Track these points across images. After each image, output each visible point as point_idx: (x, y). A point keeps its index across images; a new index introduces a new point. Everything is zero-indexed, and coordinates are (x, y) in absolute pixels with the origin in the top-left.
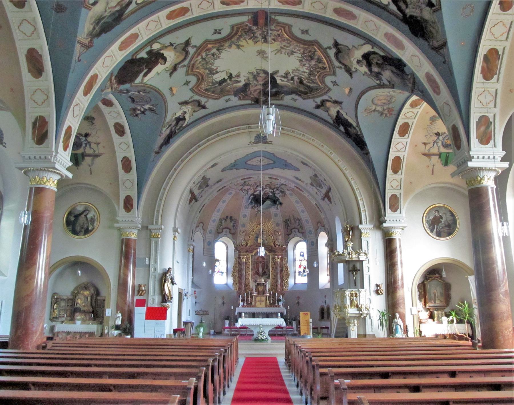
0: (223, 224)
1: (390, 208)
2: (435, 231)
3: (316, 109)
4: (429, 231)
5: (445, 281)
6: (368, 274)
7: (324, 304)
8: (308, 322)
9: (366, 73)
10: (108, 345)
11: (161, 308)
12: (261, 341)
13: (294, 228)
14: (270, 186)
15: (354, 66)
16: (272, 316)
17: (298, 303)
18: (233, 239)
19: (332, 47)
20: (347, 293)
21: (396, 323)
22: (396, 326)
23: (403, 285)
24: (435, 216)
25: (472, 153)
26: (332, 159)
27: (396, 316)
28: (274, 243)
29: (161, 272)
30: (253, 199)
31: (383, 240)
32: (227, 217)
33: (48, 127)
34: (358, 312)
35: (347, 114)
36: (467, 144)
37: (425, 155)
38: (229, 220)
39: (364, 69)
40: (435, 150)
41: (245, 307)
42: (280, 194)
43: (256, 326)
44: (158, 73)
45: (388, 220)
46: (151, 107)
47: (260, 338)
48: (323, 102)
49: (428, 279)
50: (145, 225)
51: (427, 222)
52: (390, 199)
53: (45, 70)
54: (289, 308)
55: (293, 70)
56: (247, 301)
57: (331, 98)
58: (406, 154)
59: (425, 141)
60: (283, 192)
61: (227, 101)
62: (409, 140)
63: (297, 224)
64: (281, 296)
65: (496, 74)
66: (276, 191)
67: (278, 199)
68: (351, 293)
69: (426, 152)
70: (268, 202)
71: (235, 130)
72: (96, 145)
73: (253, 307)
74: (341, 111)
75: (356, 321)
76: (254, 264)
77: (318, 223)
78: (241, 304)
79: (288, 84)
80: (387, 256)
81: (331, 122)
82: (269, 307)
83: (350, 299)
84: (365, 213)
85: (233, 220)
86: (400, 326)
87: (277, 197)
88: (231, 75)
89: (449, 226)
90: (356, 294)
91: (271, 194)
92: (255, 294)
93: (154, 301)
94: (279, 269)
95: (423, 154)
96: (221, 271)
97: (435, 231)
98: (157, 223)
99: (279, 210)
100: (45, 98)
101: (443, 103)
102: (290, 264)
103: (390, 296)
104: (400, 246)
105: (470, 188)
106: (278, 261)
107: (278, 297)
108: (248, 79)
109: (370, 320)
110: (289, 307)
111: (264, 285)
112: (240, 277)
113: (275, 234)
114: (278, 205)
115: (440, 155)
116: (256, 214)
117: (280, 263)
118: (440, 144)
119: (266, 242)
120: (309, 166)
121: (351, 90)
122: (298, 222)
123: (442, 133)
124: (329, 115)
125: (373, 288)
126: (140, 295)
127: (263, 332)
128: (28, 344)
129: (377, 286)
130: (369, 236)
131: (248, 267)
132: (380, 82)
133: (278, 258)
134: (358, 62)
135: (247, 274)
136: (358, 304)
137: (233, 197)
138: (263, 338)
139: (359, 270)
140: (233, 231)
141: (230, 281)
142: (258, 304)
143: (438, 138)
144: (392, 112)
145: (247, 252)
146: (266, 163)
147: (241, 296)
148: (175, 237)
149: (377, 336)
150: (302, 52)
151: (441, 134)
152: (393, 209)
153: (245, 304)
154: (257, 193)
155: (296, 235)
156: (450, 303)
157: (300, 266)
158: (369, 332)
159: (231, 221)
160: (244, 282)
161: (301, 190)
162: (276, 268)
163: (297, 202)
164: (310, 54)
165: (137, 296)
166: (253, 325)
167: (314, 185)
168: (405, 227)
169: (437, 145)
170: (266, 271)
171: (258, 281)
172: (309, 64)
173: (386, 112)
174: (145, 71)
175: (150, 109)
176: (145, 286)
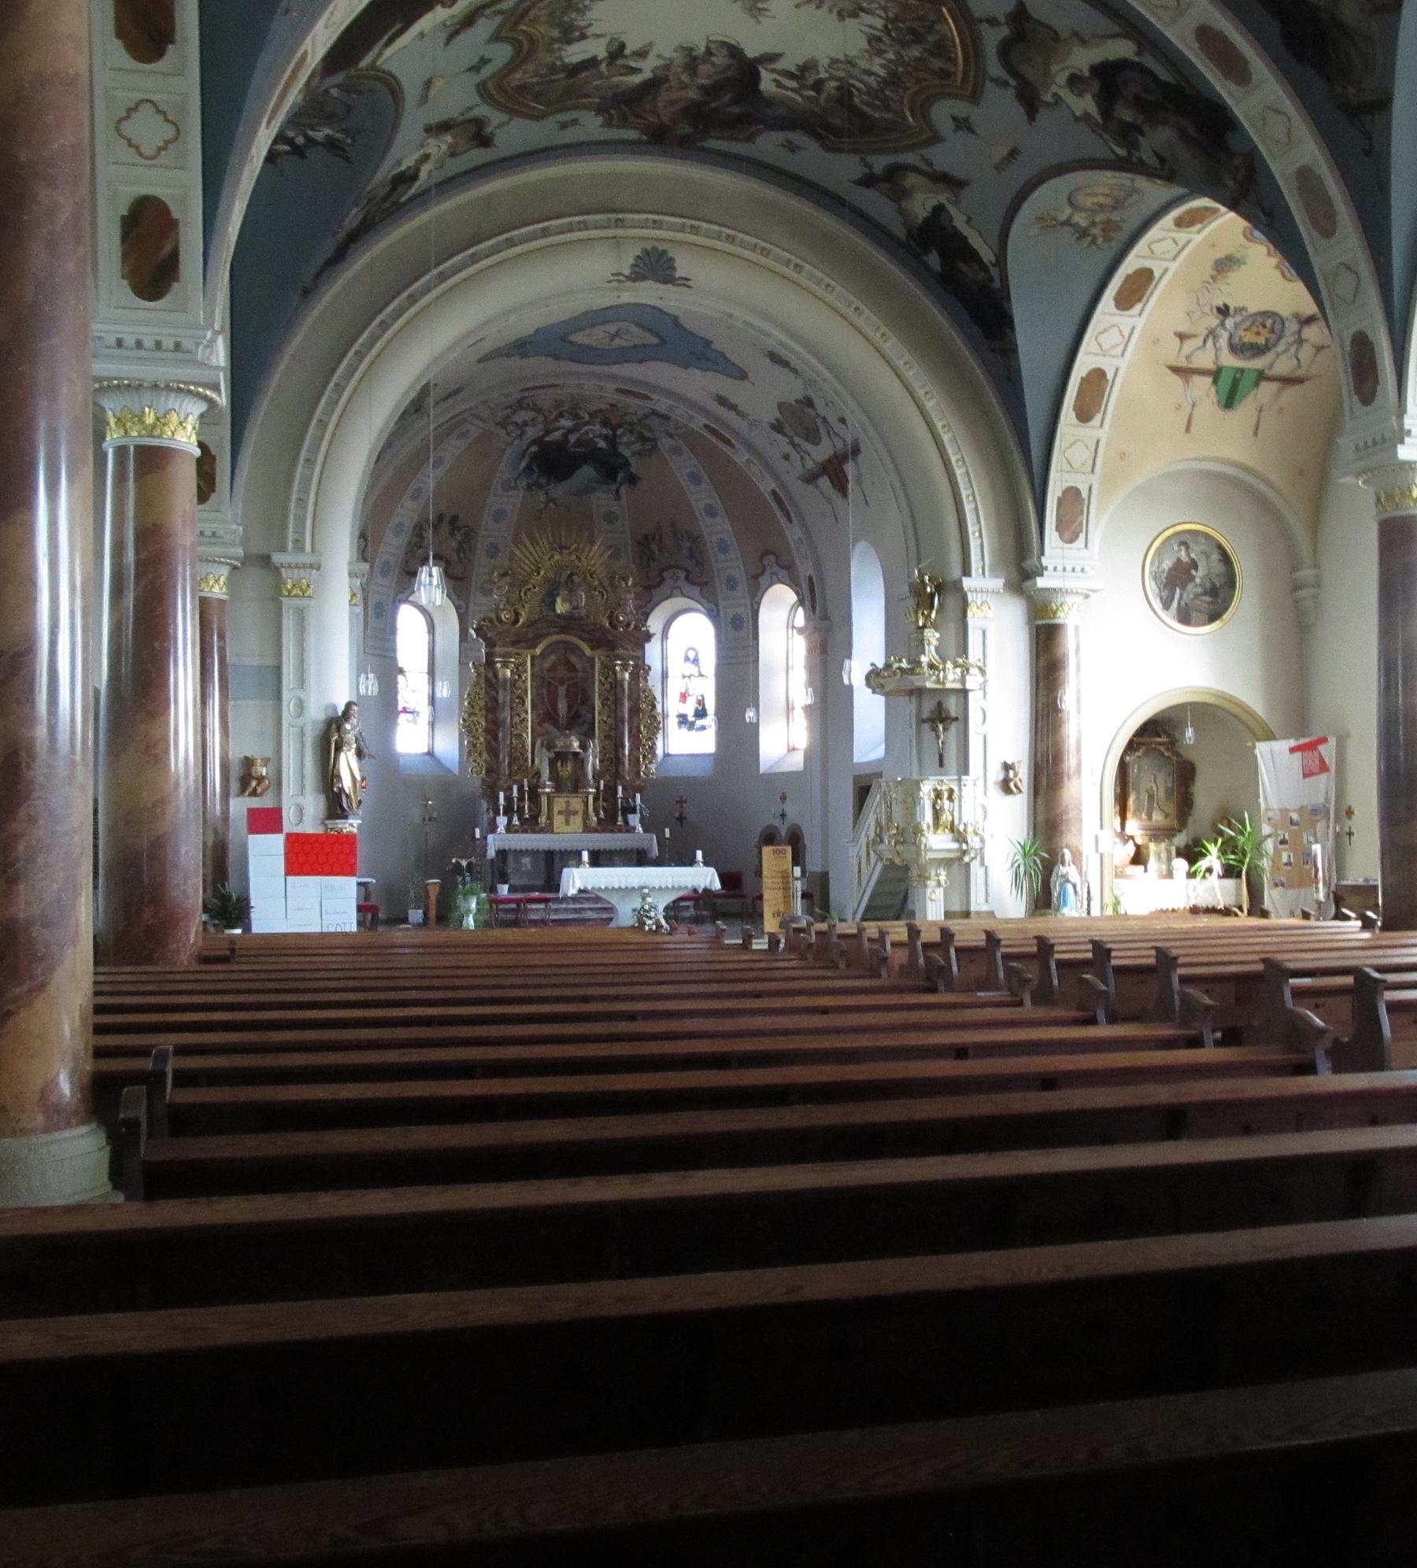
3: (862, 189)
4: (1157, 605)
5: (1181, 756)
6: (983, 730)
7: (777, 822)
9: (1086, 117)
10: (322, 948)
11: (327, 836)
14: (609, 419)
15: (1054, 89)
16: (610, 859)
19: (1002, 20)
20: (926, 789)
21: (1063, 876)
22: (1062, 885)
23: (1079, 765)
25: (1045, 561)
26: (883, 357)
27: (1063, 856)
30: (535, 457)
31: (1026, 629)
33: (177, 239)
34: (955, 846)
35: (969, 221)
36: (1397, 396)
37: (1176, 370)
38: (445, 528)
39: (1086, 104)
40: (1205, 360)
41: (516, 832)
42: (637, 447)
43: (627, 891)
44: (422, 35)
45: (1050, 567)
46: (338, 135)
48: (894, 174)
49: (1138, 749)
50: (256, 548)
51: (1155, 577)
52: (1060, 502)
53: (178, 37)
54: (667, 835)
55: (834, 62)
56: (521, 810)
57: (931, 165)
58: (1123, 364)
59: (1183, 328)
60: (648, 439)
61: (564, 126)
62: (1140, 323)
64: (638, 796)
66: (623, 434)
67: (627, 464)
68: (935, 790)
69: (1182, 362)
70: (587, 472)
71: (570, 229)
73: (542, 831)
74: (950, 208)
75: (943, 873)
76: (537, 688)
78: (502, 821)
79: (797, 98)
80: (1037, 679)
81: (901, 233)
82: (596, 831)
85: (459, 531)
86: (1074, 886)
87: (624, 457)
88: (622, 46)
89: (1213, 592)
90: (951, 791)
91: (602, 444)
92: (547, 790)
93: (300, 812)
98: (299, 546)
99: (624, 502)
100: (170, 132)
101: (1334, 264)
103: (1040, 800)
104: (1077, 650)
105: (1385, 516)
106: (623, 680)
107: (625, 798)
108: (667, 67)
109: (983, 869)
111: (578, 760)
112: (492, 732)
114: (621, 484)
115: (1216, 374)
116: (540, 511)
117: (629, 683)
118: (1223, 342)
119: (583, 613)
120: (795, 371)
121: (1014, 153)
124: (901, 212)
125: (996, 774)
126: (249, 795)
128: (178, 951)
129: (1007, 767)
130: (990, 614)
131: (519, 697)
132: (1130, 154)
133: (625, 667)
134: (1074, 81)
135: (517, 719)
136: (956, 822)
139: (956, 719)
142: (558, 820)
144: (1112, 234)
145: (514, 644)
146: (632, 344)
149: (999, 915)
150: (891, 15)
151: (1231, 312)
152: (1067, 535)
153: (516, 821)
154: (557, 435)
155: (676, 591)
156: (1191, 820)
157: (684, 697)
158: (977, 903)
159: (452, 534)
160: (507, 750)
161: (729, 443)
162: (618, 702)
163: (695, 479)
164: (915, 25)
165: (238, 795)
166: (620, 888)
167: (787, 429)
168: (1094, 591)
170: (583, 711)
171: (559, 743)
172: (898, 53)
173: (1096, 231)
174: (398, 26)
175: (331, 144)
176: (266, 762)
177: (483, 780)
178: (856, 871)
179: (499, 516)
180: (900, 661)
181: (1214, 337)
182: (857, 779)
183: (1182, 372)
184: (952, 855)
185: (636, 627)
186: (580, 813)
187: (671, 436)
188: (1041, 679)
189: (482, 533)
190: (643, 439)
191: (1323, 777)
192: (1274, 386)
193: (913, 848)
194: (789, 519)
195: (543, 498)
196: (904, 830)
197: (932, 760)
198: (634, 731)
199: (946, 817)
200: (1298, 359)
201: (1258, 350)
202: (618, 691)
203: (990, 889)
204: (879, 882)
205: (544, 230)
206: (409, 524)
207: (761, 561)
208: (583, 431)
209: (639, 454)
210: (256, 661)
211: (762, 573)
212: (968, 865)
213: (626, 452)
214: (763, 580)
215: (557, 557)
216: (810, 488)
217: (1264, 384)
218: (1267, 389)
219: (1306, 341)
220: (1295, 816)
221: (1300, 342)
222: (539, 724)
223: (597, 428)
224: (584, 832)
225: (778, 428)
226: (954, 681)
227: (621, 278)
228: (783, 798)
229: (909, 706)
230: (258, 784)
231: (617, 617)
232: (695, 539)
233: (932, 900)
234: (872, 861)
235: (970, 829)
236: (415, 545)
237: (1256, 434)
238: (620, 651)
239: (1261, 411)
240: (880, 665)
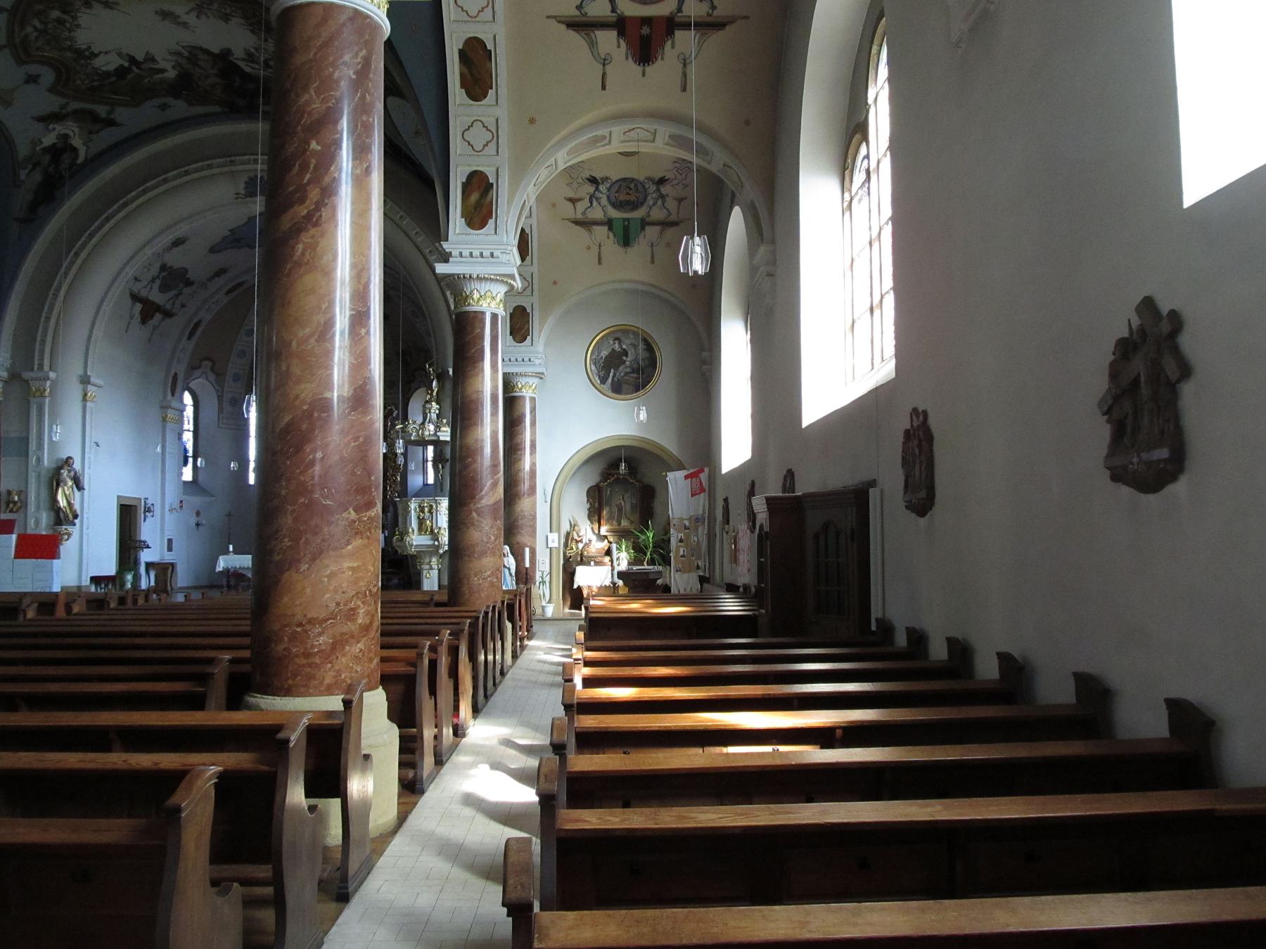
2: (610, 380)
24: (613, 349)
29: (54, 466)
37: (577, 223)
40: (597, 213)
51: (595, 362)
65: (492, 88)
68: (420, 506)
71: (201, 169)
72: (675, 203)
83: (419, 517)
93: (37, 523)
95: (573, 222)
97: (610, 380)
98: (41, 366)
115: (609, 223)
118: (604, 201)
123: (602, 179)
136: (434, 527)
143: (597, 189)
165: (5, 512)
169: (599, 204)
181: (597, 199)
183: (585, 224)
191: (702, 495)
192: (658, 228)
200: (666, 208)
201: (634, 206)
205: (186, 171)
207: (201, 361)
217: (648, 228)
218: (652, 232)
219: (667, 195)
220: (687, 523)
221: (663, 197)
227: (242, 196)
237: (653, 262)
239: (652, 246)
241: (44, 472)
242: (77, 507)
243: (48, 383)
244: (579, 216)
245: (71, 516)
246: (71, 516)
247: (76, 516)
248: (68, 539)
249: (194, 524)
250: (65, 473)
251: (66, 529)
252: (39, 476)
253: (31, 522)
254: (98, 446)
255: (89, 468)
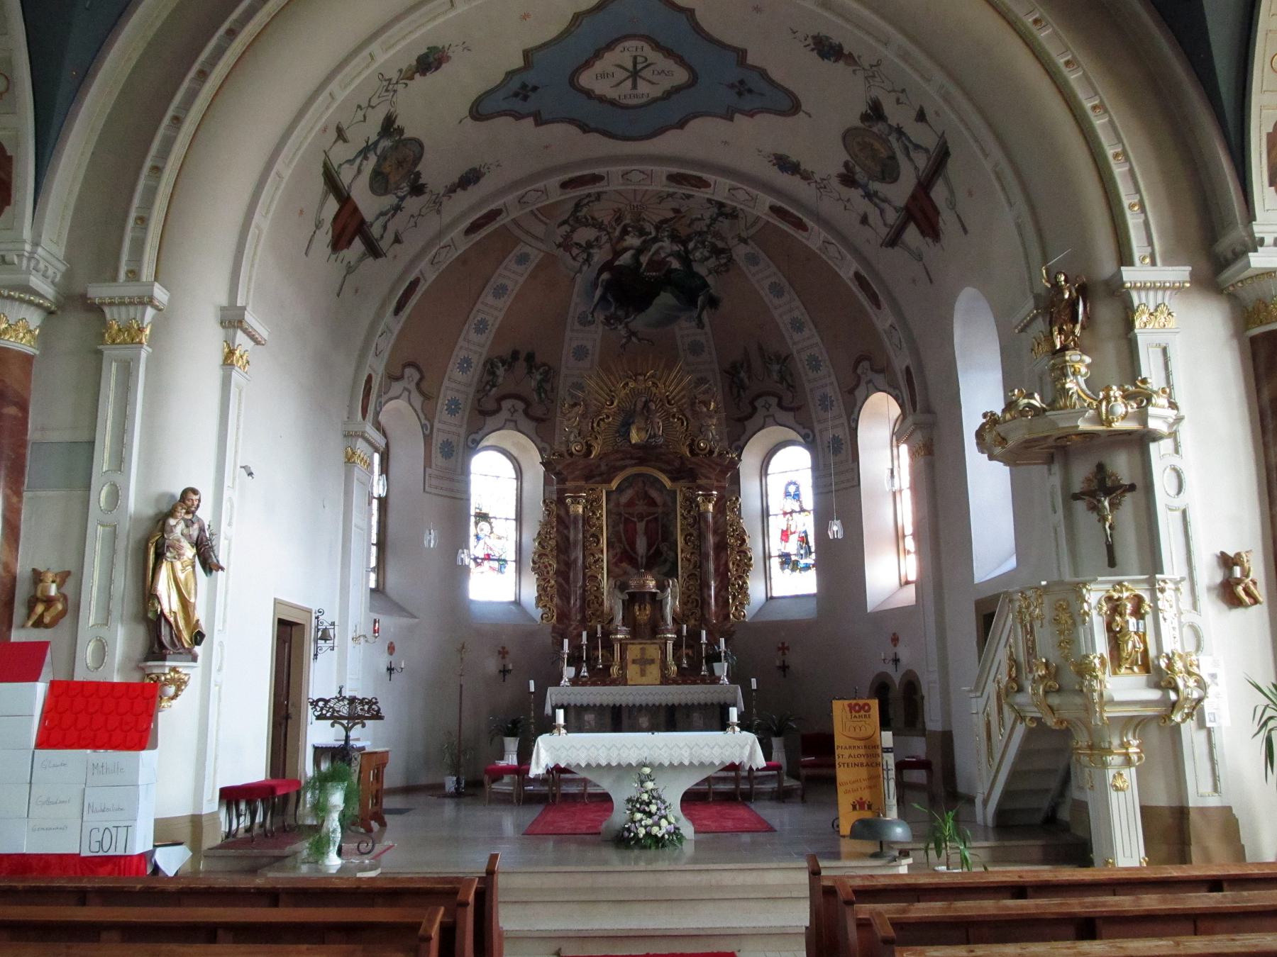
0: (500, 380)
1: (1271, 184)
6: (1179, 502)
7: (889, 668)
8: (872, 748)
12: (644, 847)
13: (759, 396)
14: (672, 227)
17: (784, 668)
18: (538, 440)
20: (1094, 596)
25: (1258, 229)
28: (691, 446)
29: (150, 511)
30: (608, 286)
31: (1235, 343)
32: (515, 355)
34: (1155, 695)
38: (521, 365)
41: (584, 684)
43: (622, 770)
47: (642, 832)
54: (754, 686)
56: (591, 661)
60: (722, 251)
63: (775, 376)
64: (722, 640)
66: (696, 248)
67: (706, 285)
70: (666, 299)
73: (614, 683)
77: (858, 363)
78: (569, 672)
80: (1262, 420)
82: (675, 682)
83: (1109, 628)
84: (1141, 219)
85: (537, 369)
87: (701, 277)
90: (1138, 601)
91: (675, 264)
93: (102, 650)
94: (711, 539)
96: (496, 553)
98: (134, 275)
99: (707, 328)
102: (750, 522)
106: (707, 511)
107: (709, 644)
109: (1203, 734)
110: (754, 680)
111: (656, 602)
112: (564, 574)
113: (695, 413)
114: (702, 309)
116: (623, 346)
119: (661, 441)
122: (776, 367)
125: (1208, 575)
127: (659, 798)
129: (1227, 562)
130: (1172, 323)
131: (593, 535)
133: (708, 498)
135: (591, 559)
136: (1152, 652)
137: (533, 276)
138: (655, 830)
139: (1132, 488)
140: (538, 411)
141: (530, 592)
142: (633, 671)
145: (588, 478)
147: (566, 642)
148: (231, 352)
153: (584, 672)
154: (626, 258)
155: (769, 420)
157: (785, 535)
159: (530, 372)
161: (800, 225)
162: (701, 537)
163: (777, 290)
165: (23, 626)
166: (609, 765)
170: (664, 548)
177: (554, 627)
178: (984, 735)
179: (581, 353)
180: (1031, 396)
182: (979, 604)
184: (1150, 712)
185: (720, 455)
186: (658, 662)
187: (744, 241)
188: (1269, 419)
189: (563, 371)
190: (717, 252)
193: (1078, 700)
194: (877, 304)
195: (623, 332)
196: (1057, 668)
197: (1093, 550)
198: (722, 568)
199: (1131, 645)
202: (702, 524)
203: (1221, 771)
204: (1023, 754)
206: (477, 361)
207: (855, 368)
208: (653, 250)
209: (716, 271)
210: (67, 436)
211: (857, 385)
212: (1176, 729)
213: (701, 269)
214: (859, 393)
215: (631, 385)
216: (896, 252)
222: (616, 564)
223: (667, 245)
224: (662, 684)
225: (848, 179)
226: (1124, 417)
228: (895, 640)
229: (1049, 480)
230: (47, 609)
231: (699, 444)
232: (784, 360)
233: (1117, 789)
234: (1009, 723)
235: (1179, 665)
236: (487, 383)
238: (702, 482)
240: (998, 407)
241: (125, 526)
242: (200, 614)
243: (150, 312)
244: (884, 231)
245: (186, 636)
246: (186, 636)
247: (198, 637)
248: (176, 696)
249: (385, 670)
250: (177, 526)
251: (174, 669)
252: (114, 535)
253: (87, 652)
254: (250, 474)
255: (230, 524)
